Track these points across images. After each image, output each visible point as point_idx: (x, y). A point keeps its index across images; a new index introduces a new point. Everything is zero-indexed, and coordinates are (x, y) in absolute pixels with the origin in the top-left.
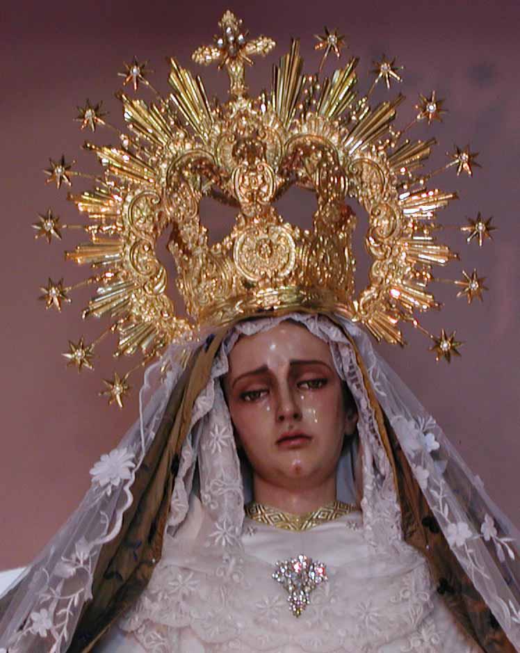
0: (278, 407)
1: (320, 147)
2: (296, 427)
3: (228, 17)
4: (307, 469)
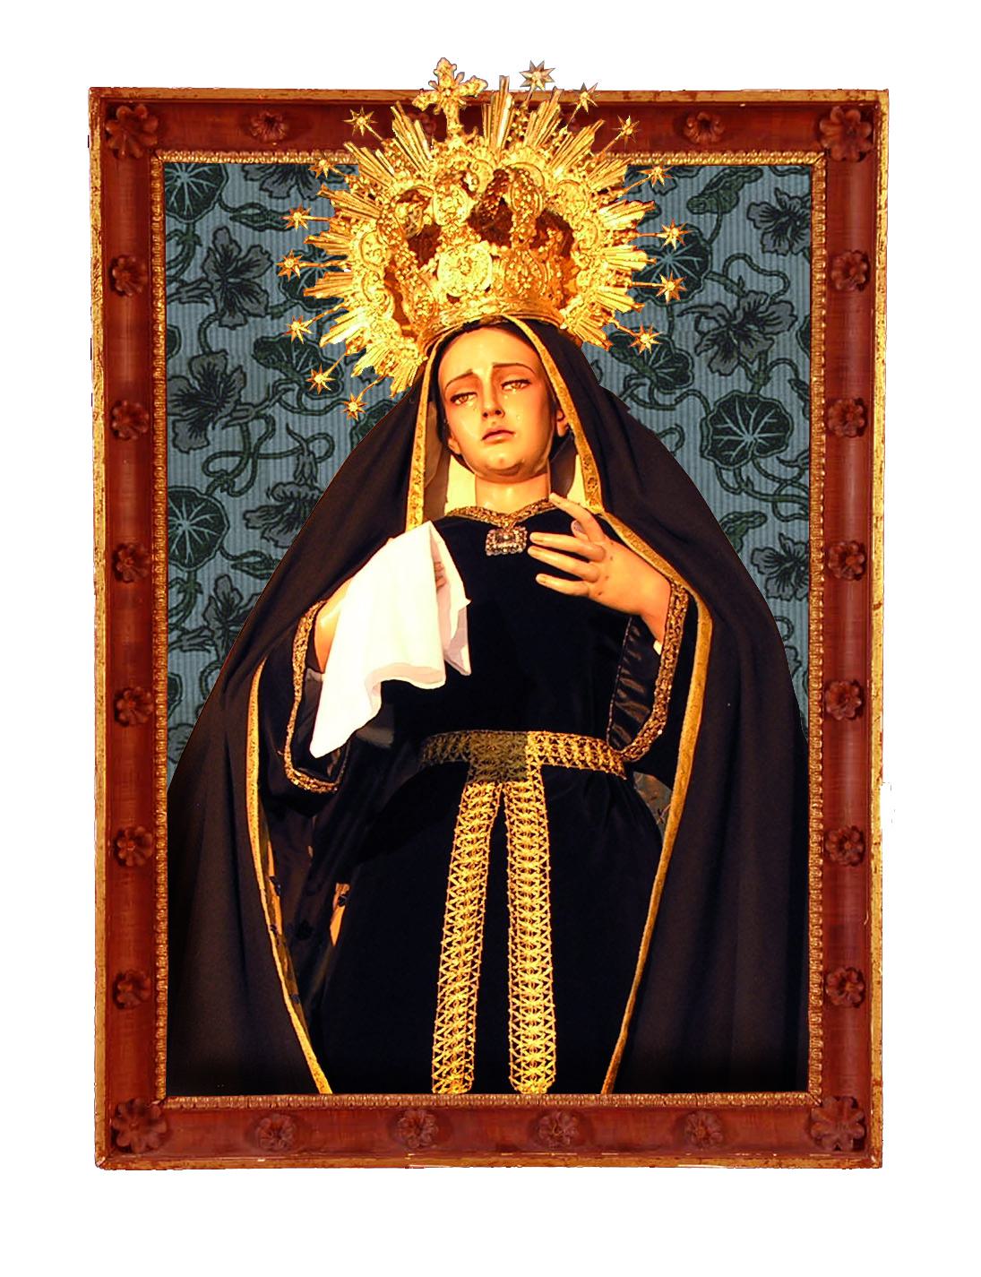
3: (640, 659)
4: (510, 462)
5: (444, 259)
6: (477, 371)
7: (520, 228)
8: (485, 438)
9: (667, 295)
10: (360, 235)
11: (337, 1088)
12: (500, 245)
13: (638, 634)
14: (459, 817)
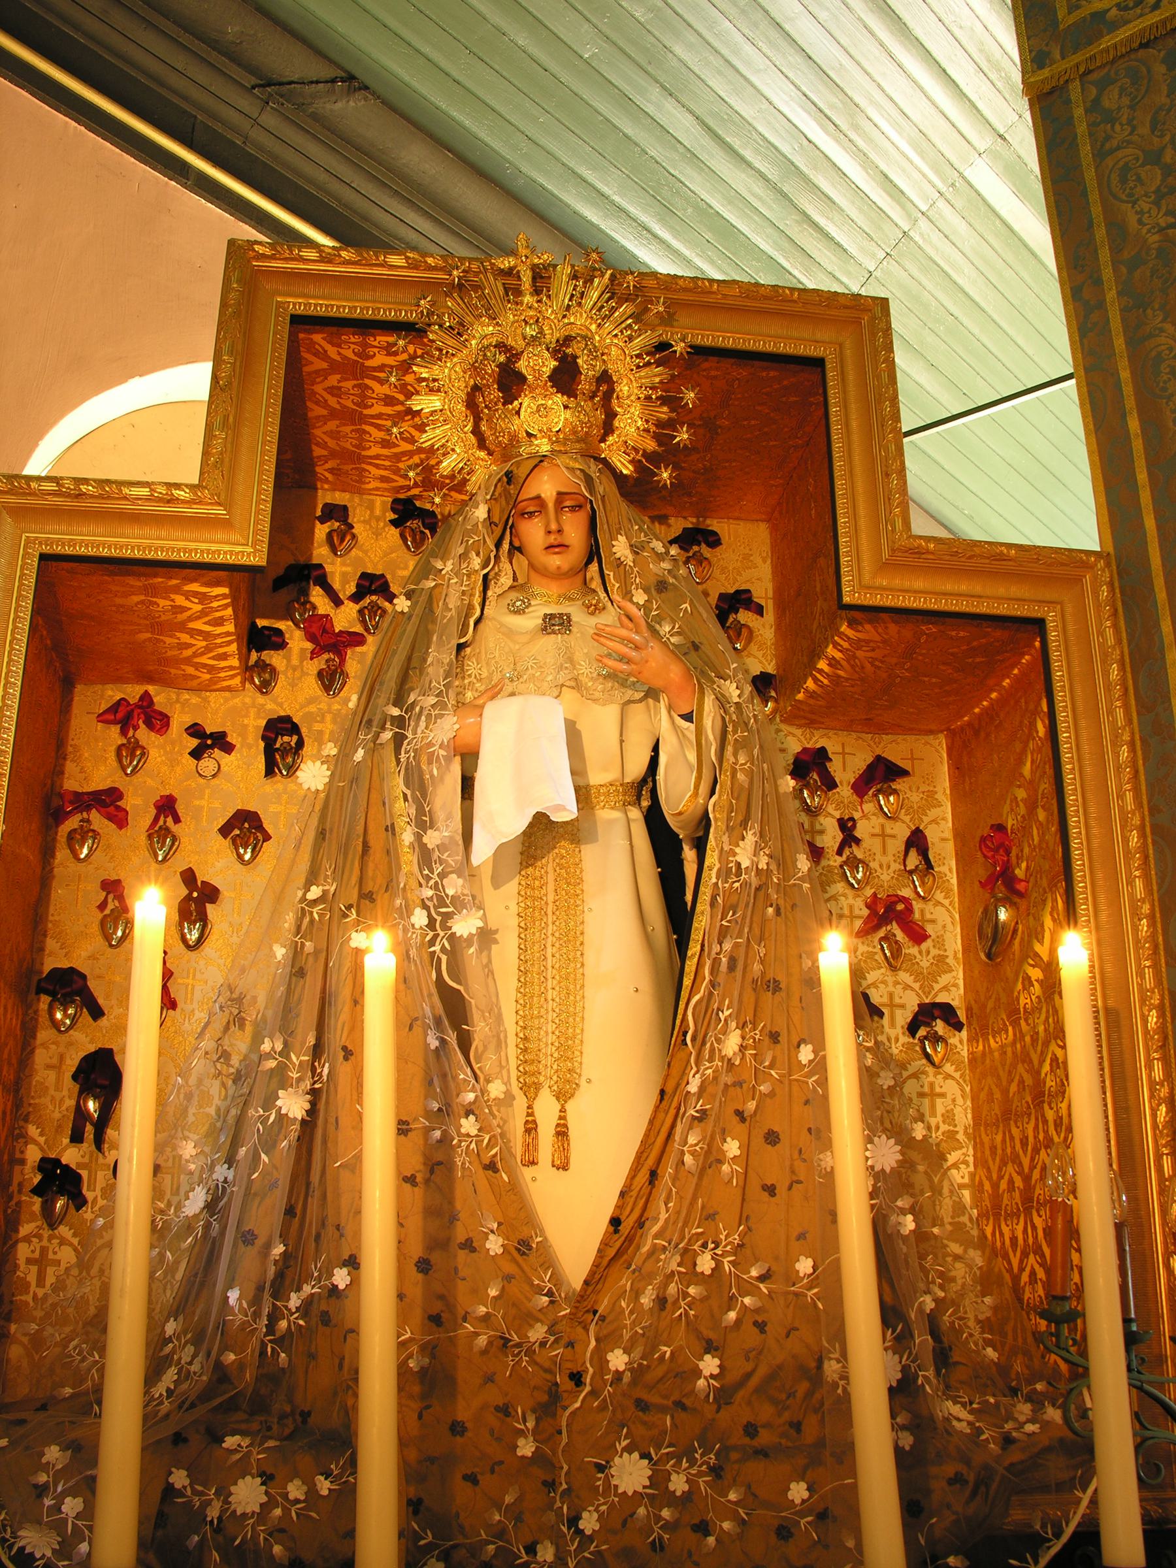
0: (547, 525)
1: (585, 338)
2: (559, 540)
4: (566, 567)
5: (526, 403)
7: (584, 386)
8: (547, 548)
9: (678, 439)
12: (569, 397)
14: (318, 469)
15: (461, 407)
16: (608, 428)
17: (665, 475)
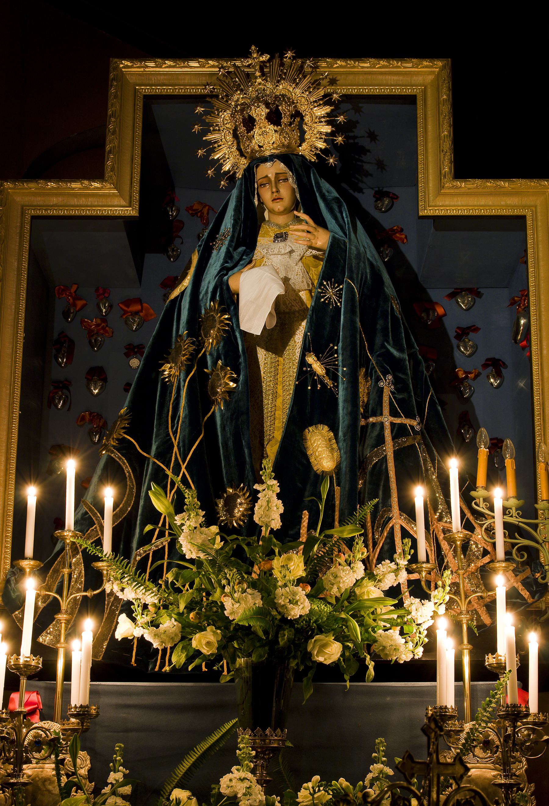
4: (282, 209)
5: (256, 130)
6: (270, 175)
8: (273, 200)
10: (223, 116)
11: (95, 524)
12: (277, 126)
13: (423, 781)
15: (230, 138)
16: (302, 139)
17: (331, 161)
